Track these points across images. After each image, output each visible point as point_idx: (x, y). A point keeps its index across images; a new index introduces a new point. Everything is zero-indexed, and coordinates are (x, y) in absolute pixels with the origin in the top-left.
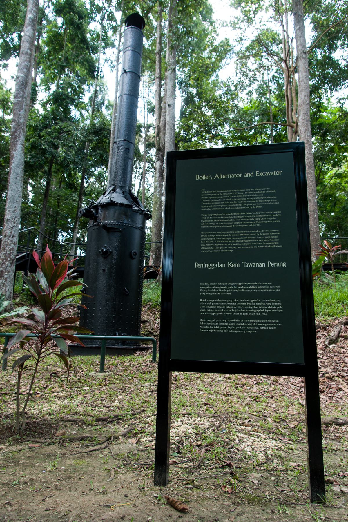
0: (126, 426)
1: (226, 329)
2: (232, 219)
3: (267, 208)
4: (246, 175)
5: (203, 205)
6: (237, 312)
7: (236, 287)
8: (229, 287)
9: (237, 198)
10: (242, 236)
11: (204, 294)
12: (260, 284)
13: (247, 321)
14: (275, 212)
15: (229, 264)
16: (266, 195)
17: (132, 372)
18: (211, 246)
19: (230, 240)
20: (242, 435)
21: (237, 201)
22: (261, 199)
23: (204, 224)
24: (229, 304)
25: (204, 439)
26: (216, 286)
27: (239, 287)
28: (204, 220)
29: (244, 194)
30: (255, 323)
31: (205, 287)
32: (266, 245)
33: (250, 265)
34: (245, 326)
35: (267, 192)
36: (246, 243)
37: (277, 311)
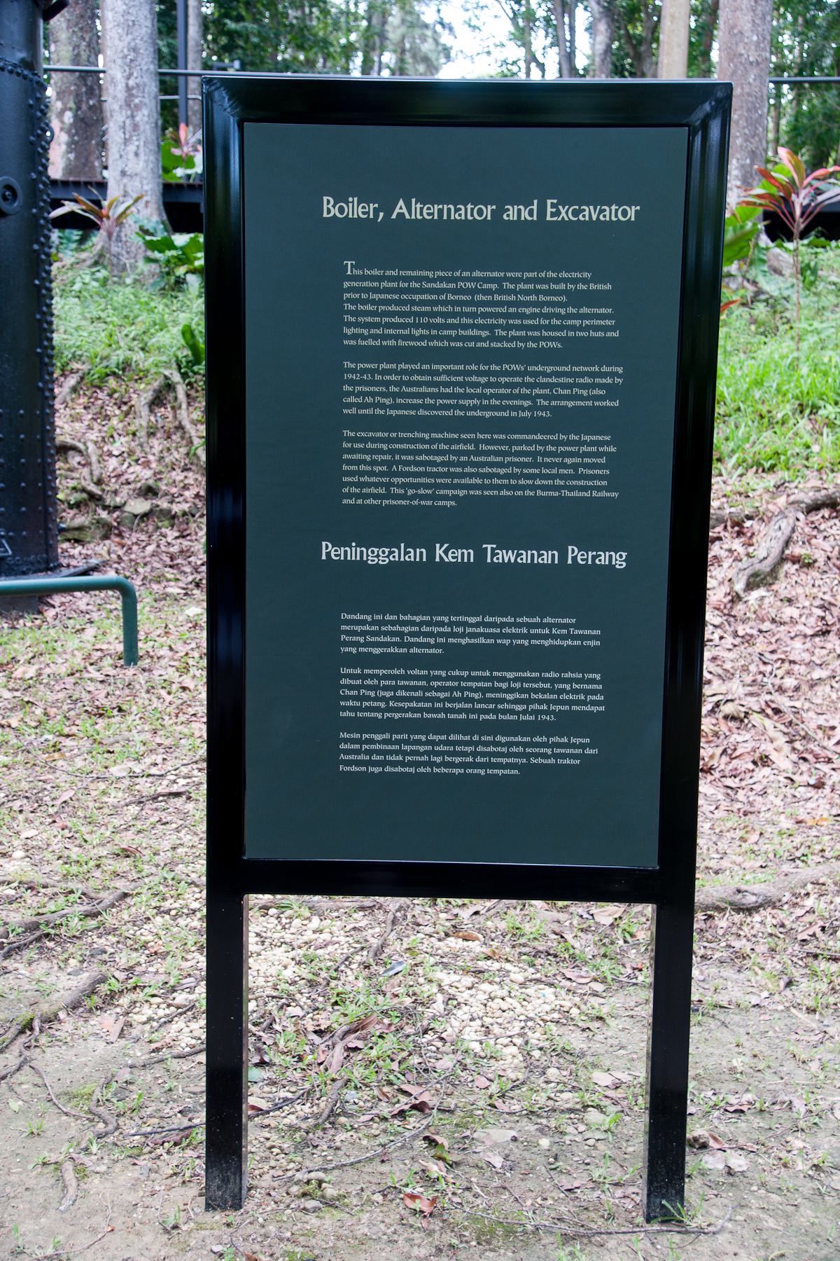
0: (72, 962)
1: (424, 764)
2: (455, 384)
3: (575, 351)
4: (511, 214)
5: (349, 325)
6: (460, 711)
7: (461, 630)
8: (435, 630)
9: (471, 303)
10: (488, 453)
11: (354, 650)
12: (538, 620)
13: (490, 738)
14: (605, 369)
15: (439, 552)
16: (577, 299)
17: (52, 711)
18: (376, 485)
19: (443, 464)
20: (454, 978)
21: (473, 315)
22: (558, 316)
23: (352, 399)
24: (435, 684)
25: (336, 1003)
26: (393, 623)
27: (469, 630)
28: (352, 383)
29: (501, 291)
30: (517, 744)
31: (358, 628)
32: (565, 487)
33: (507, 556)
34: (483, 754)
35: (581, 286)
36: (499, 476)
37: (589, 708)
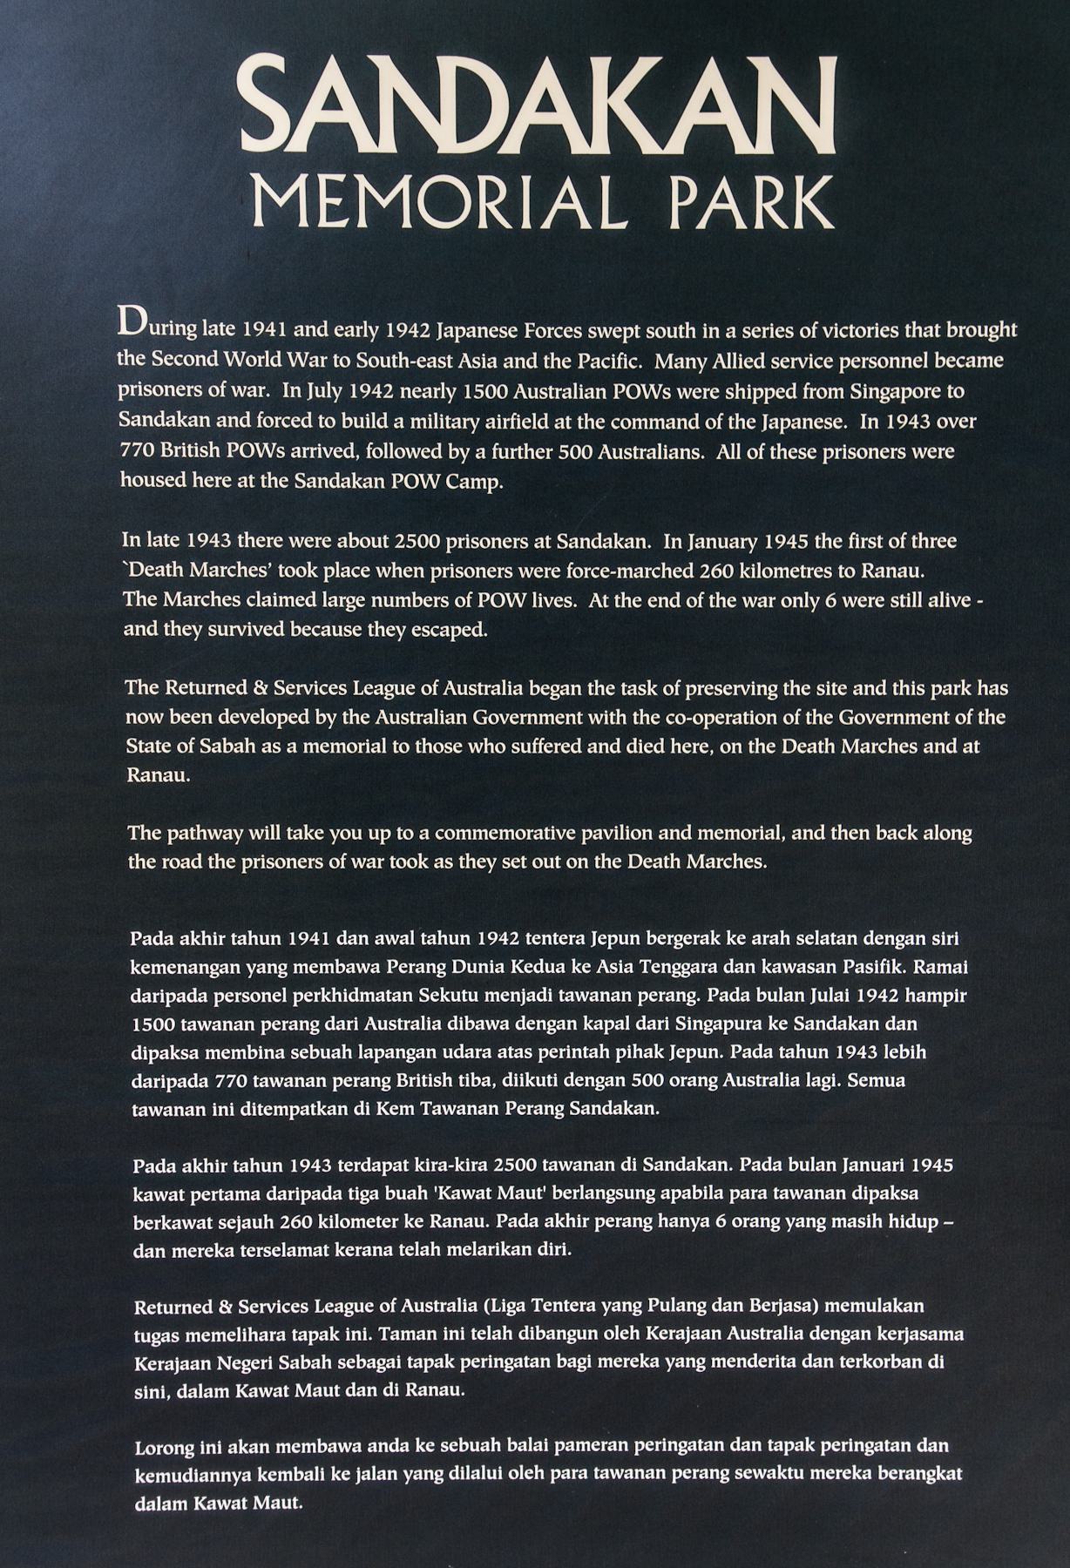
5: (131, 374)
